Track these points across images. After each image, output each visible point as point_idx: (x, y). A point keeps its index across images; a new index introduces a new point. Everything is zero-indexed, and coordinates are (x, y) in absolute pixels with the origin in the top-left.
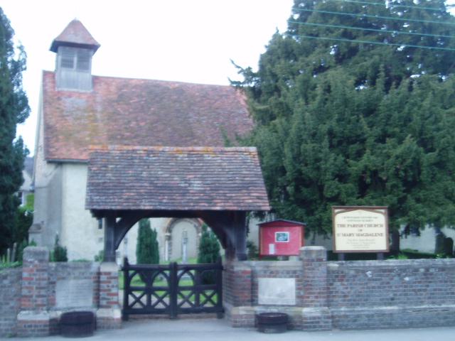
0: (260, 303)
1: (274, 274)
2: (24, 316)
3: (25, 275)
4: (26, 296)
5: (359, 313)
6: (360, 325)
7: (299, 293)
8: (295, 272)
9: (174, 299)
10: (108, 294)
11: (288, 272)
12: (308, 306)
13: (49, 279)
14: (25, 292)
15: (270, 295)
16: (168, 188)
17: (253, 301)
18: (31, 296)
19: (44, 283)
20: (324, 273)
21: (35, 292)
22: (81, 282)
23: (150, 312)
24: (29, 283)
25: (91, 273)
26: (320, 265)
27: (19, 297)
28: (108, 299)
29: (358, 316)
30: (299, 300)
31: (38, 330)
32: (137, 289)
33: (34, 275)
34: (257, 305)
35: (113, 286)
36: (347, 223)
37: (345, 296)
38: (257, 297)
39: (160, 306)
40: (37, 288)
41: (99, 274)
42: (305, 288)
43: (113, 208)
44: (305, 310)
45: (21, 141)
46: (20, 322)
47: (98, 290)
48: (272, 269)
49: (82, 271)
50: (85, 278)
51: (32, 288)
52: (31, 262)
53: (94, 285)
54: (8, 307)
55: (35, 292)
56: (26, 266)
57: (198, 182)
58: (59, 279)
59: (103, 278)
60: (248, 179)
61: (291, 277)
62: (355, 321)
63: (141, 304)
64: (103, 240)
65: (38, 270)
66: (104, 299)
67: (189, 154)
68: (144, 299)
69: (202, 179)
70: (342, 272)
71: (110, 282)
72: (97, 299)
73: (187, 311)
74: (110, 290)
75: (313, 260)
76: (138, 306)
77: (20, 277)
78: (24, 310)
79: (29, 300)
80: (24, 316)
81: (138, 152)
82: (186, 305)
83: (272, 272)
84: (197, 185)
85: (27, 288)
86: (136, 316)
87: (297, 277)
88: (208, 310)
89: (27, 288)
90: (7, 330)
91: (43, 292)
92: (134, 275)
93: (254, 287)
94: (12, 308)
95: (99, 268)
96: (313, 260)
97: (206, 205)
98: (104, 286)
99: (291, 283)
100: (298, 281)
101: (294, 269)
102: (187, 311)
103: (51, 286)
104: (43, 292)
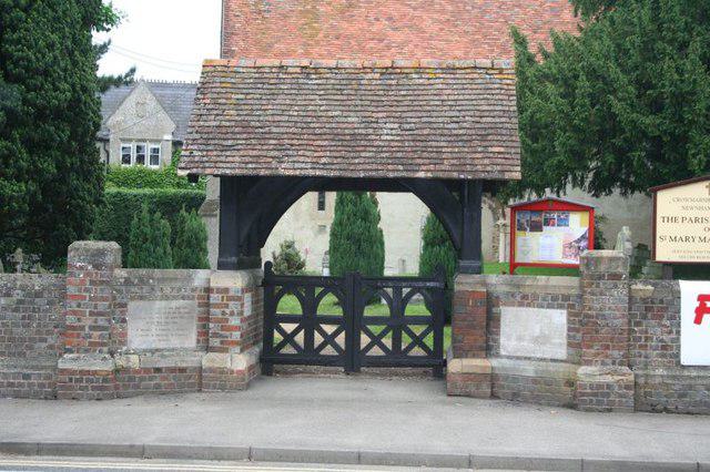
0: (503, 352)
1: (526, 300)
2: (67, 362)
3: (71, 290)
4: (74, 328)
5: (693, 382)
6: (696, 404)
7: (574, 337)
8: (566, 298)
9: (353, 340)
10: (223, 328)
11: (555, 298)
12: (588, 363)
13: (114, 298)
14: (71, 320)
15: (520, 339)
16: (353, 142)
17: (489, 349)
18: (83, 328)
19: (102, 306)
20: (621, 301)
21: (88, 321)
22: (174, 304)
23: (309, 359)
24: (79, 306)
25: (193, 290)
26: (616, 286)
27: (66, 331)
28: (221, 336)
29: (691, 387)
30: (572, 351)
31: (93, 388)
32: (289, 319)
33: (86, 290)
34: (498, 355)
35: (232, 314)
36: (680, 214)
37: (664, 348)
38: (496, 341)
39: (329, 351)
40: (91, 314)
41: (208, 290)
42: (584, 331)
43: (692, 260)
44: (582, 370)
45: (104, 48)
46: (63, 371)
47: (205, 320)
48: (527, 291)
49: (179, 284)
50: (183, 298)
51: (83, 314)
52: (81, 268)
53: (197, 311)
54: (44, 345)
55: (88, 321)
56: (72, 274)
57: (392, 126)
58: (132, 299)
59: (215, 298)
60: (489, 119)
61: (561, 307)
62: (682, 396)
63: (296, 346)
64: (328, 230)
65: (92, 282)
66: (216, 335)
67: (382, 74)
68: (300, 338)
69: (401, 120)
70: (662, 301)
71: (227, 306)
72: (204, 333)
73: (376, 362)
74: (227, 320)
75: (601, 277)
76: (288, 350)
77: (63, 296)
78: (71, 351)
79: (78, 335)
80: (67, 362)
81: (290, 70)
82: (376, 351)
83: (524, 297)
84: (389, 131)
85: (74, 313)
86: (290, 368)
87: (571, 306)
88: (415, 363)
89: (74, 313)
90: (42, 386)
91: (102, 322)
92: (322, 295)
93: (491, 322)
94: (51, 347)
95: (209, 281)
96: (601, 277)
97: (401, 167)
98: (216, 312)
99: (559, 317)
100: (569, 314)
101: (565, 292)
102: (376, 362)
103: (118, 311)
104: (102, 322)
